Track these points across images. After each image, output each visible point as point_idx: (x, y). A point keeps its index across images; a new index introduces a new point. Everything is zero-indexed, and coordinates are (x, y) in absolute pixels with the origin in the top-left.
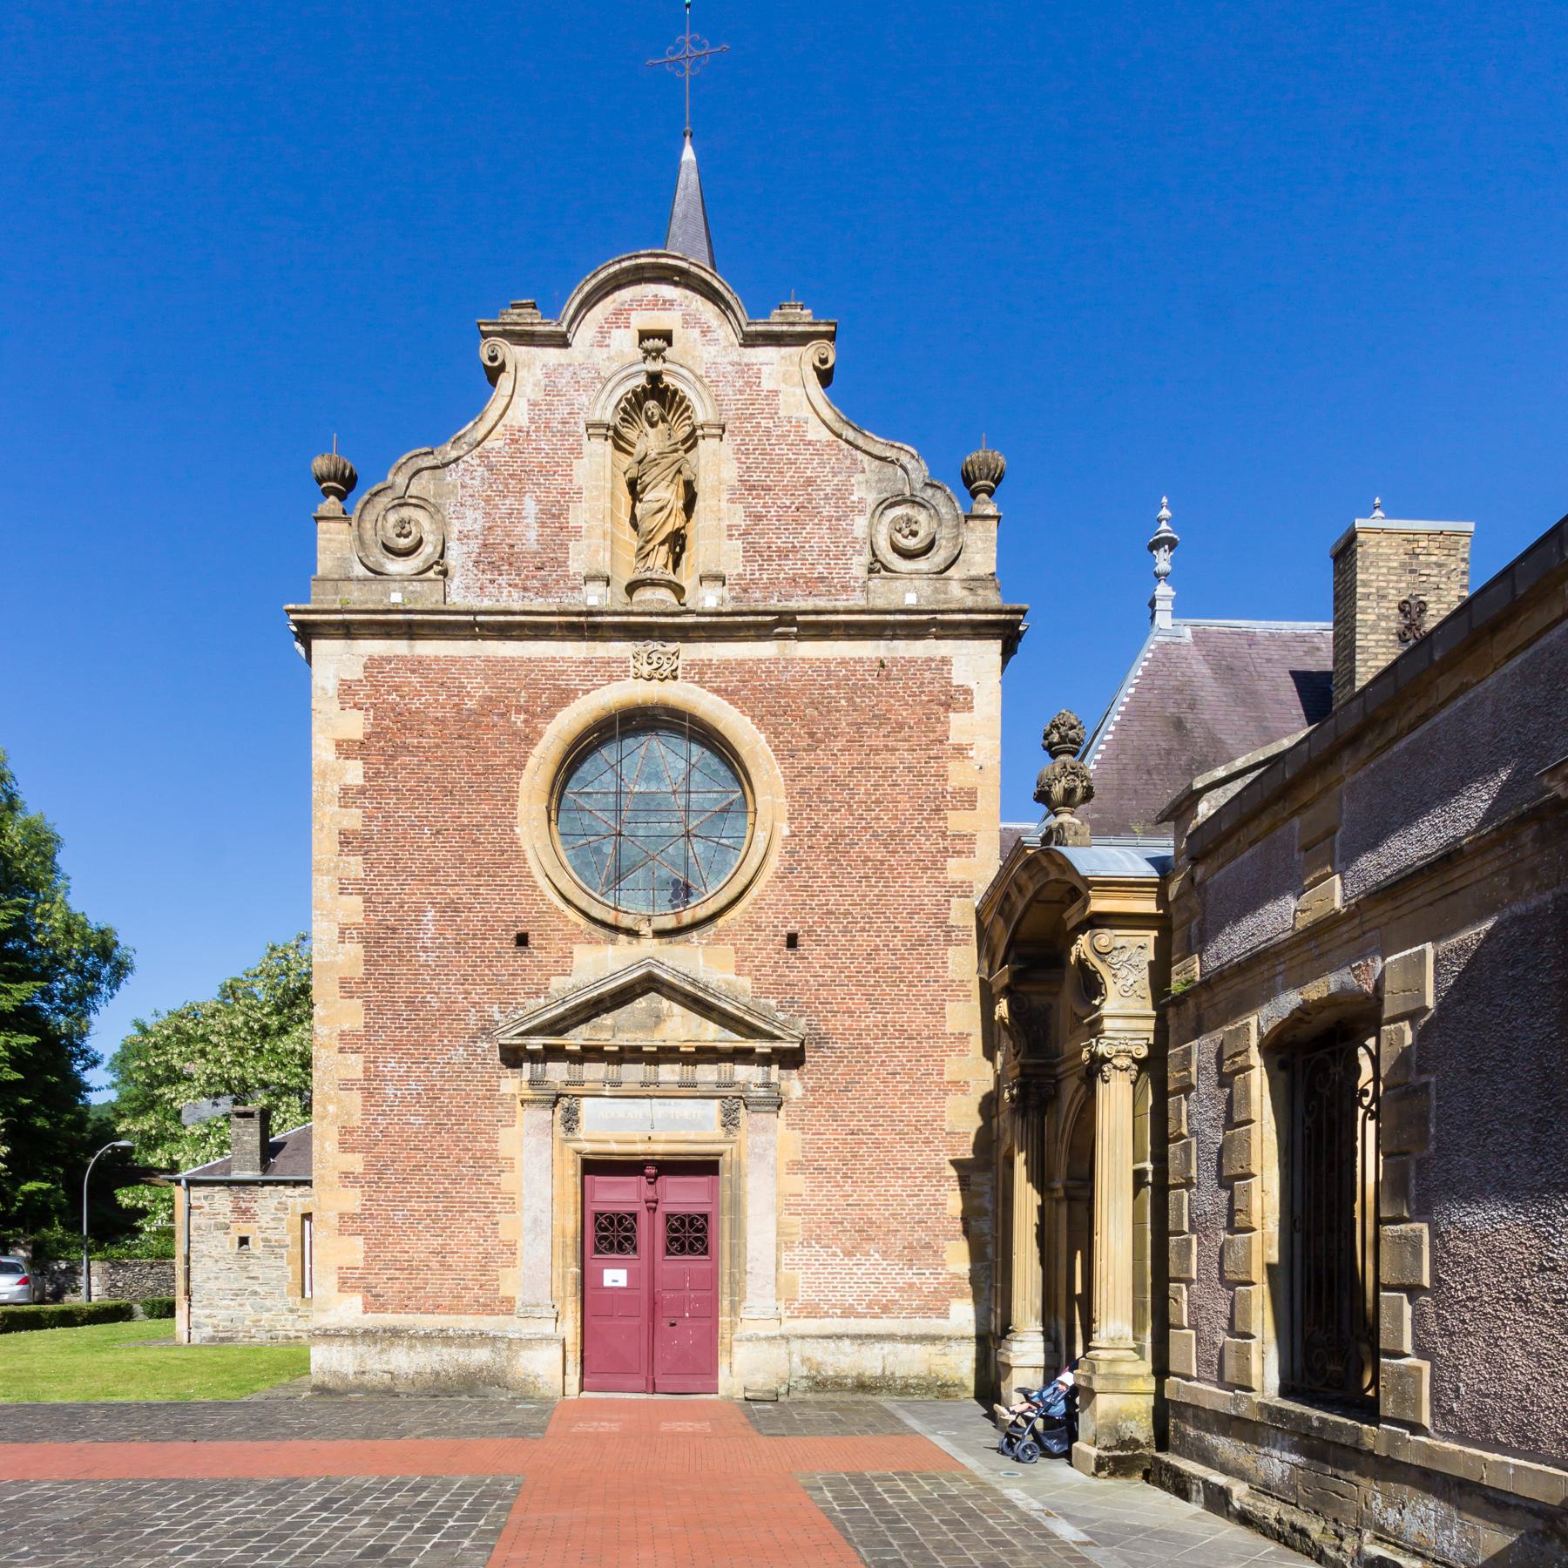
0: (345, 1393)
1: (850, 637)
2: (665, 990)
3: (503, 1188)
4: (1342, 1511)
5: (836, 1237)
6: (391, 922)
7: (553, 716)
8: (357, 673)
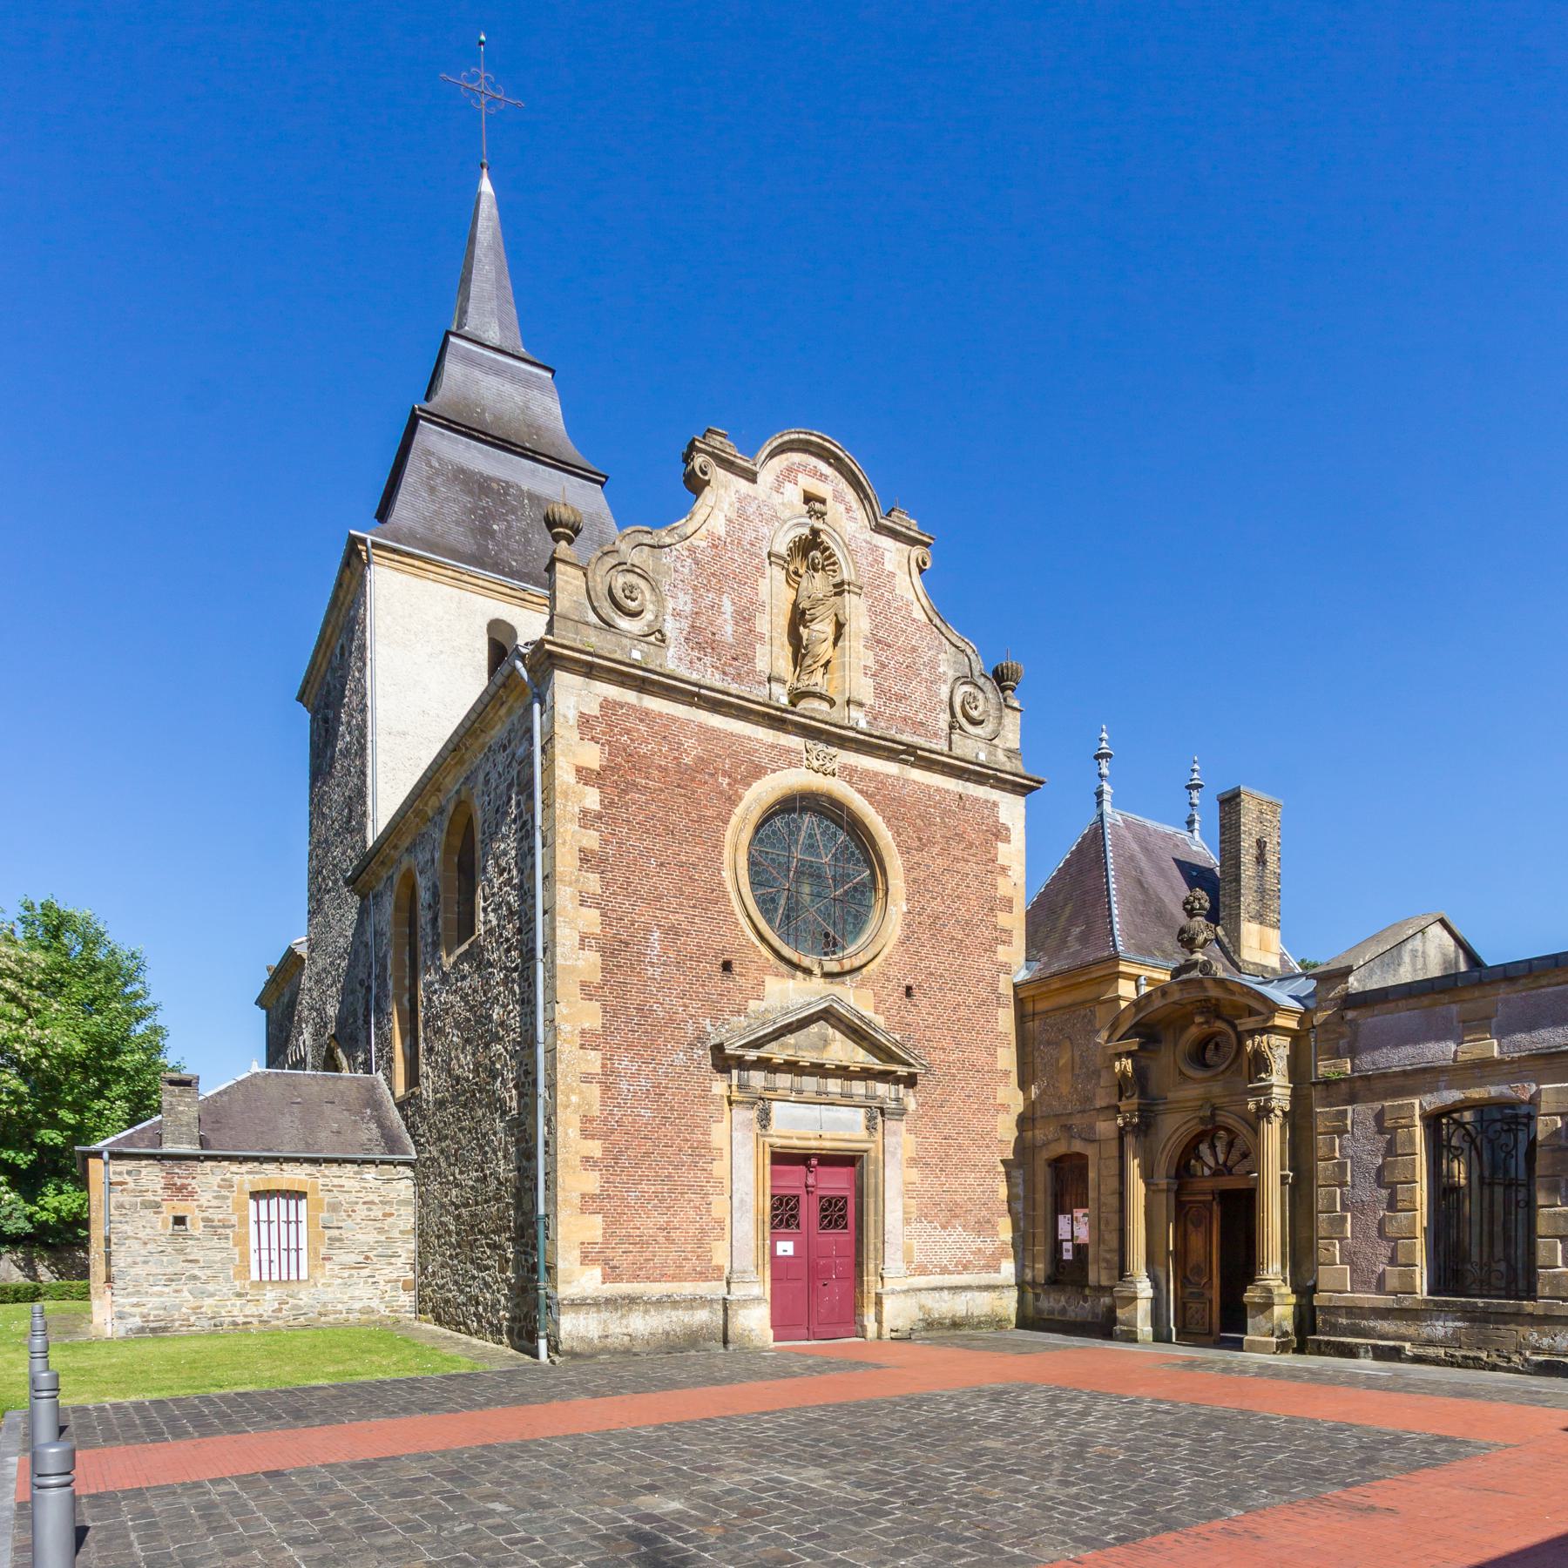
0: (592, 1356)
1: (943, 773)
2: (833, 1021)
3: (715, 1173)
4: (1503, 1343)
5: (936, 1215)
6: (624, 937)
7: (750, 785)
8: (593, 709)
